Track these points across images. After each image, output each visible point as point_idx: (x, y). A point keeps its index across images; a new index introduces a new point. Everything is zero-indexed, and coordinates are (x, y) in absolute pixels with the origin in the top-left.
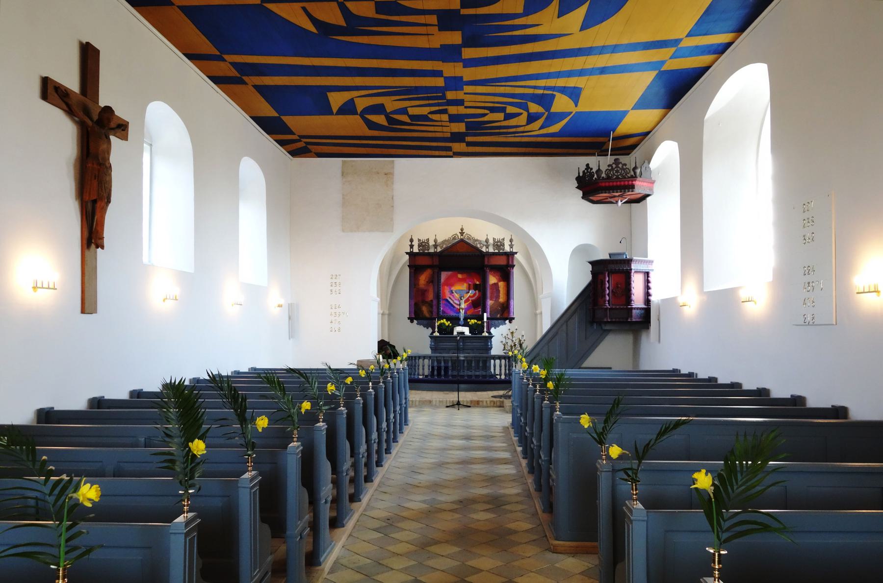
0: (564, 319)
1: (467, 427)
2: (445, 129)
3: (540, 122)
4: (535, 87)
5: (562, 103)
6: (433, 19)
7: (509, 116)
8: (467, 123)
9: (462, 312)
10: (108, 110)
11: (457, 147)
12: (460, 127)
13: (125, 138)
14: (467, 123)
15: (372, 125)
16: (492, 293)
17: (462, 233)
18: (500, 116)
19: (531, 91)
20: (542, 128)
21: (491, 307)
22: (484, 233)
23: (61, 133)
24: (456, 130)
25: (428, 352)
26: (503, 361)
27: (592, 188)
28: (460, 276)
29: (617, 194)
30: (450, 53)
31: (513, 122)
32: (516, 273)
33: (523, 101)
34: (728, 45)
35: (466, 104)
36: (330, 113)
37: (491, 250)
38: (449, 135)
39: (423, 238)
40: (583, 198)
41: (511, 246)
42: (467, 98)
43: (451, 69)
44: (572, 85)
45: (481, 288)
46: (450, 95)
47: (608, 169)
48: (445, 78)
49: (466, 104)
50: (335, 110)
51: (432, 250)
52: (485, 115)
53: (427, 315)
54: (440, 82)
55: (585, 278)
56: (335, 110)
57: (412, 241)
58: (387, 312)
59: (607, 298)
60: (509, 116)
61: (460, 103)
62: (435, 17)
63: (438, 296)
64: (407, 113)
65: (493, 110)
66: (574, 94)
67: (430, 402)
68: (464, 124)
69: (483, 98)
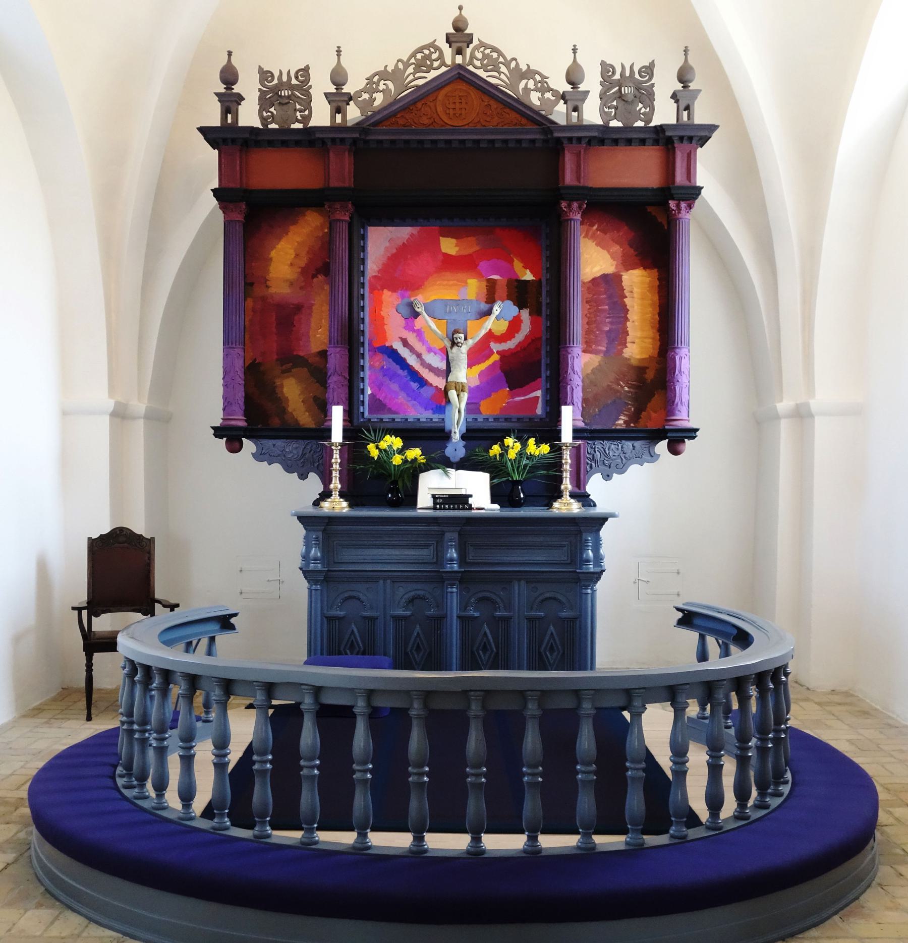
9: (459, 402)
39: (284, 65)
45: (546, 299)
58: (140, 406)
63: (350, 335)
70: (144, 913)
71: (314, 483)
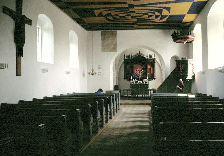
1: (138, 111)
2: (131, 21)
3: (159, 18)
4: (156, 7)
5: (165, 12)
7: (149, 16)
8: (137, 18)
9: (140, 77)
10: (24, 16)
11: (135, 26)
12: (135, 20)
13: (31, 25)
14: (137, 18)
15: (109, 20)
16: (149, 71)
17: (140, 53)
18: (147, 16)
19: (155, 8)
20: (160, 20)
21: (149, 75)
22: (147, 53)
23: (10, 24)
24: (134, 21)
25: (130, 88)
26: (153, 91)
27: (176, 38)
28: (139, 66)
29: (184, 40)
31: (151, 18)
32: (156, 64)
33: (153, 11)
35: (136, 13)
36: (96, 17)
37: (148, 58)
38: (132, 22)
39: (128, 55)
40: (174, 41)
41: (154, 57)
42: (136, 10)
44: (167, 6)
45: (145, 69)
46: (131, 10)
47: (180, 30)
49: (136, 13)
50: (97, 16)
51: (130, 58)
52: (142, 16)
54: (127, 6)
55: (175, 66)
56: (97, 16)
57: (124, 55)
58: (118, 77)
59: (181, 72)
60: (149, 16)
61: (134, 12)
63: (132, 72)
64: (118, 16)
65: (144, 14)
66: (168, 9)
67: (128, 103)
68: (136, 19)
69: (141, 11)
70: (210, 123)
71: (130, 82)
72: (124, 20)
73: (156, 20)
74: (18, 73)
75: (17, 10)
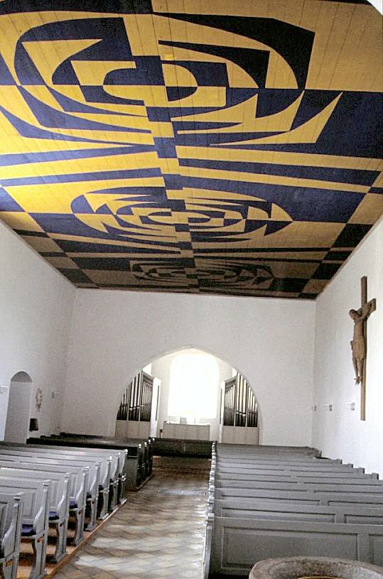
0: (229, 99)
6: (188, 207)
20: (236, 282)
30: (175, 182)
34: (150, 215)
42: (145, 123)
43: (170, 166)
48: (176, 157)
53: (330, 231)
54: (183, 151)
60: (228, 222)
62: (187, 208)
72: (269, 472)
73: (245, 236)
74: (363, 418)
75: (305, 294)
